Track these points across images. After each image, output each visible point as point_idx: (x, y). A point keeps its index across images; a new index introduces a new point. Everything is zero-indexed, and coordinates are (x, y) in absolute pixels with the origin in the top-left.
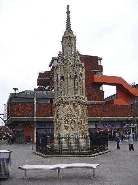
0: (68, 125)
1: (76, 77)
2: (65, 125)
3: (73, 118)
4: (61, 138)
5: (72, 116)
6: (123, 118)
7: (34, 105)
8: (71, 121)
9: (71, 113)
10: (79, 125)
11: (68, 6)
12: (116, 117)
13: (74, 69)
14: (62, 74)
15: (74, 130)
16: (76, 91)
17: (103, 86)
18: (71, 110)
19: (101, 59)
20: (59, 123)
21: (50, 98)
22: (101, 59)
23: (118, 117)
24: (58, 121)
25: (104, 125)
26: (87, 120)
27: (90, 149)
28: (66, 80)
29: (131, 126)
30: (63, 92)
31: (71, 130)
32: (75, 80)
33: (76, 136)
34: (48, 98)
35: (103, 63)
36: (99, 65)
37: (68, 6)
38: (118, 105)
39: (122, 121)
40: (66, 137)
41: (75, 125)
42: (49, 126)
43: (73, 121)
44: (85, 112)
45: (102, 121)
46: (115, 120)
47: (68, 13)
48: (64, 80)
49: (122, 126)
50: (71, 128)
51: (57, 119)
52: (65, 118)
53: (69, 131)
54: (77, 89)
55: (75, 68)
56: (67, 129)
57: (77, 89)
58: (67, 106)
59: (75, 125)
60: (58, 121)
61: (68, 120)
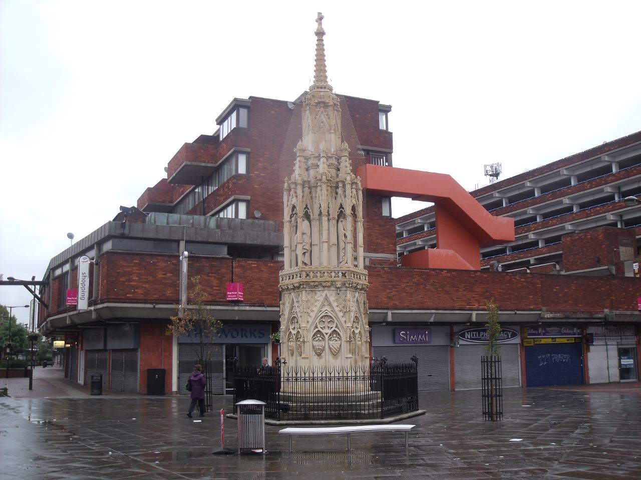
0: (322, 343)
1: (341, 215)
2: (315, 343)
3: (334, 325)
4: (339, 379)
5: (333, 322)
6: (456, 315)
7: (178, 264)
8: (330, 335)
9: (330, 314)
10: (350, 344)
11: (320, 19)
12: (433, 311)
13: (337, 193)
14: (307, 205)
15: (337, 358)
16: (342, 254)
17: (394, 200)
18: (330, 305)
19: (387, 109)
20: (297, 338)
21: (229, 240)
22: (387, 109)
23: (440, 311)
24: (294, 332)
25: (394, 334)
26: (365, 331)
27: (382, 405)
28: (317, 223)
29: (479, 339)
30: (307, 255)
31: (331, 357)
32: (340, 222)
33: (324, 375)
34: (224, 240)
35: (393, 123)
36: (382, 131)
37: (320, 19)
38: (441, 270)
39: (451, 324)
40: (349, 375)
41: (340, 346)
42: (226, 336)
43: (335, 336)
44: (362, 310)
45: (389, 324)
46: (432, 320)
47: (320, 34)
48: (310, 221)
49: (452, 340)
50: (331, 351)
51: (291, 327)
52: (316, 327)
53: (324, 359)
54: (345, 248)
55: (340, 191)
56: (319, 355)
57: (345, 248)
58: (320, 296)
59: (340, 346)
60: (294, 332)
61: (324, 331)
